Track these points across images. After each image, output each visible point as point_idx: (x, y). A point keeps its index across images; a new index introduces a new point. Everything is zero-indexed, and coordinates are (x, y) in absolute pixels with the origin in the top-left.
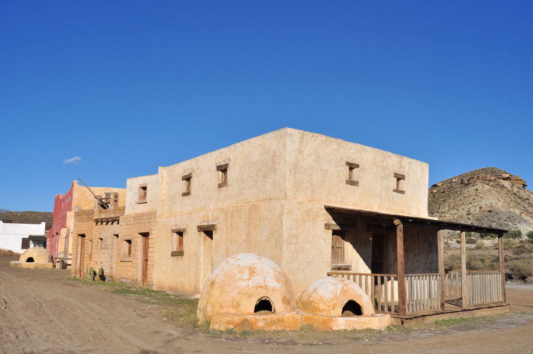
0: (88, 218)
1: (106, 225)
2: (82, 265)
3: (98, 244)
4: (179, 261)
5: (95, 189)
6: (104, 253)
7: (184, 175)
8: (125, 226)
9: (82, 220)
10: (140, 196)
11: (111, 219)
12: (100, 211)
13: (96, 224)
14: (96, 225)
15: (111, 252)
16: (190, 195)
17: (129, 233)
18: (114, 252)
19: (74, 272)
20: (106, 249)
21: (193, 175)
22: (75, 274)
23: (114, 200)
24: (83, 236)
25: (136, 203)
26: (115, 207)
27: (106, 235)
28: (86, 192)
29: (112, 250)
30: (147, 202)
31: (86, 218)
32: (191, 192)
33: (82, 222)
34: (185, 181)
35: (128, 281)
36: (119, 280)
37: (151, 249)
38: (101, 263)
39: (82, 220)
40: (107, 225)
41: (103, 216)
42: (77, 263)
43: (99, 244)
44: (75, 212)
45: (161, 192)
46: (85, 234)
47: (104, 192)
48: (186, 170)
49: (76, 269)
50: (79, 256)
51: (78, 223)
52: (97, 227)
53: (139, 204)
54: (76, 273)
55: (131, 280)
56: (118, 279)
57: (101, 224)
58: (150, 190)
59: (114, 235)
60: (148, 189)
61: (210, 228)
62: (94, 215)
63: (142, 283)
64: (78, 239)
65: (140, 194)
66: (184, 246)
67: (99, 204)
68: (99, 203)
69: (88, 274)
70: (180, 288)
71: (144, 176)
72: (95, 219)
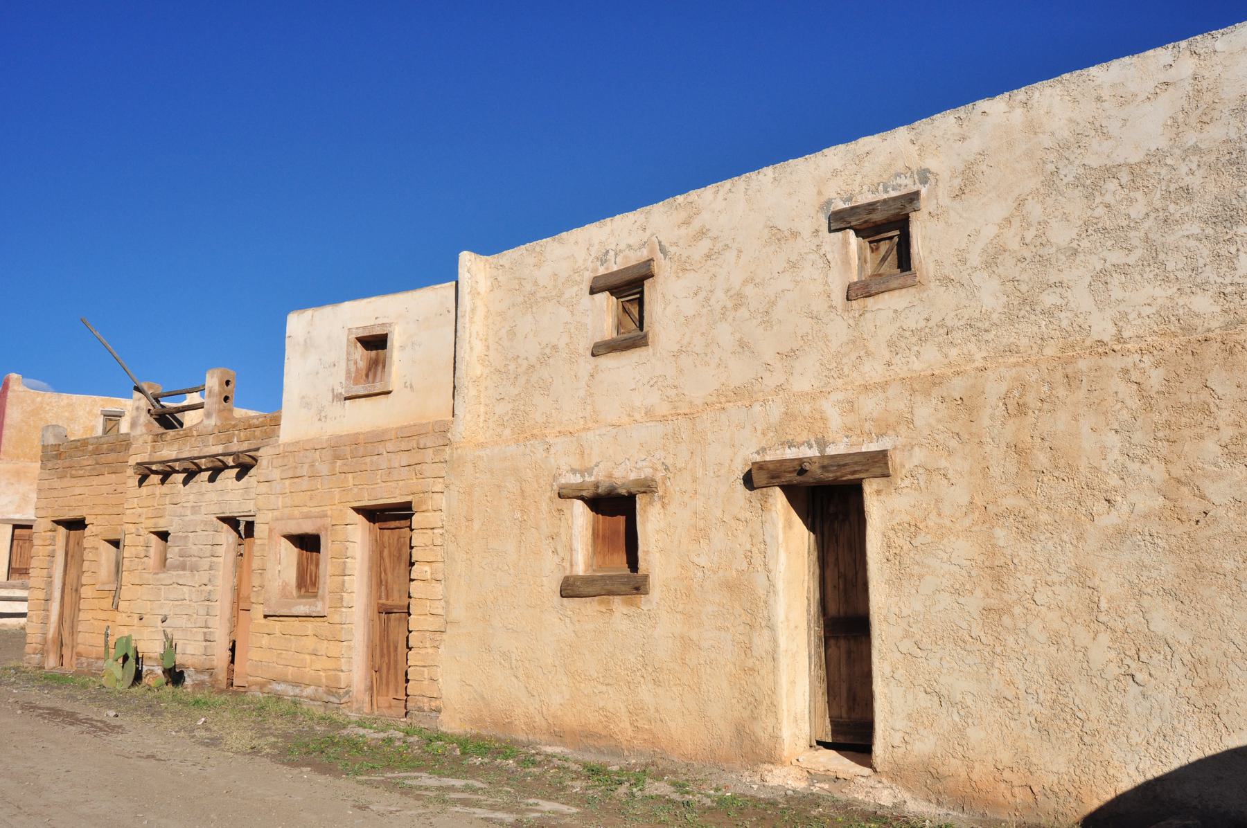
0: (97, 464)
1: (185, 482)
2: (67, 625)
3: (147, 551)
4: (617, 614)
5: (74, 401)
6: (176, 586)
7: (602, 271)
8: (287, 482)
9: (74, 472)
10: (353, 369)
11: (212, 461)
12: (157, 438)
13: (141, 482)
14: (140, 486)
15: (210, 580)
16: (646, 345)
17: (305, 509)
18: (219, 581)
19: (36, 649)
20: (184, 569)
21: (662, 267)
22: (39, 656)
23: (220, 394)
24: (76, 525)
25: (336, 397)
26: (227, 419)
27: (187, 519)
28: (48, 408)
29: (212, 572)
30: (389, 392)
31: (89, 462)
32: (650, 335)
33: (73, 477)
34: (604, 298)
35: (305, 694)
36: (262, 686)
37: (427, 568)
38: (163, 622)
39: (74, 472)
40: (191, 483)
41: (169, 452)
42: (48, 617)
43: (152, 551)
44: (43, 446)
45: (471, 348)
46: (84, 519)
47: (101, 409)
48: (612, 253)
49: (45, 639)
50: (57, 594)
51: (57, 483)
52: (145, 490)
53: (347, 402)
54: (43, 652)
55: (320, 690)
56: (256, 684)
57: (163, 481)
58: (402, 348)
59: (218, 518)
60: (395, 341)
61: (848, 469)
62: (131, 451)
63: (367, 699)
64: (54, 537)
65: (356, 363)
66: (647, 553)
67: (149, 410)
68: (151, 408)
69: (110, 661)
70: (630, 732)
71: (373, 299)
72: (138, 464)
